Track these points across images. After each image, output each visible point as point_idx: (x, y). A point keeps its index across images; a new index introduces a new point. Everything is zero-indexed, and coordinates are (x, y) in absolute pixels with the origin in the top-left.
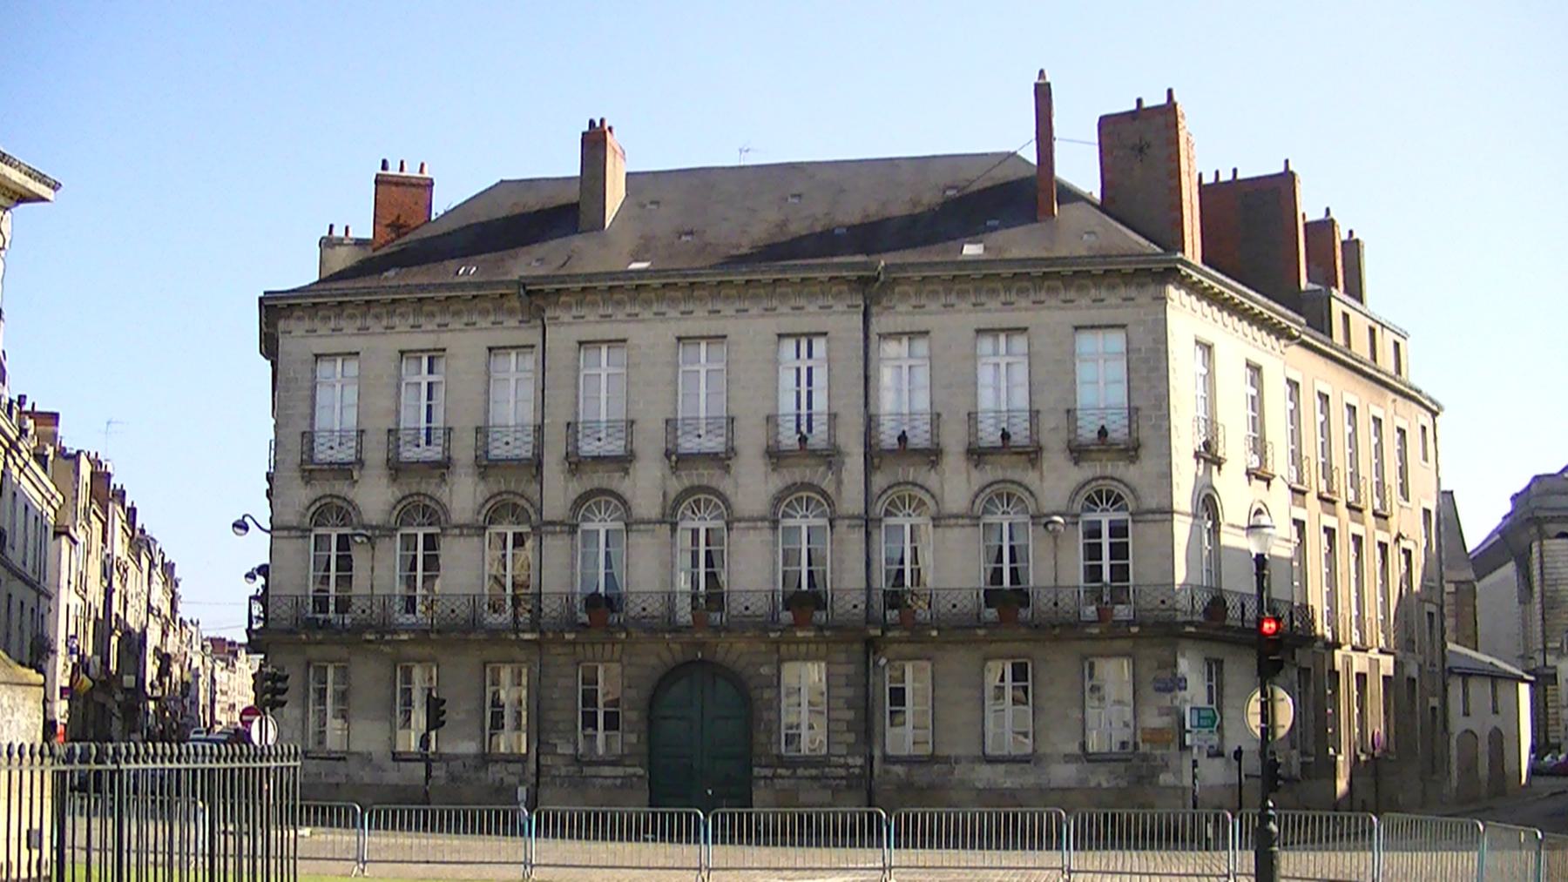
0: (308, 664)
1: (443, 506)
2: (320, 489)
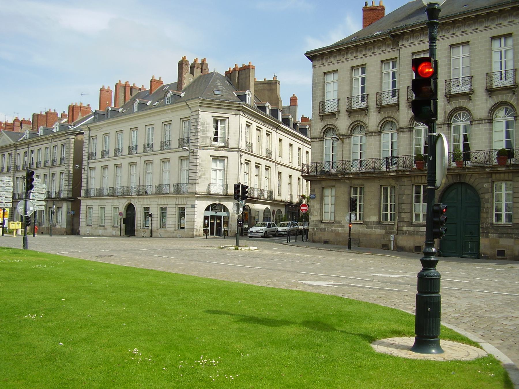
0: (381, 186)
1: (366, 125)
2: (326, 122)
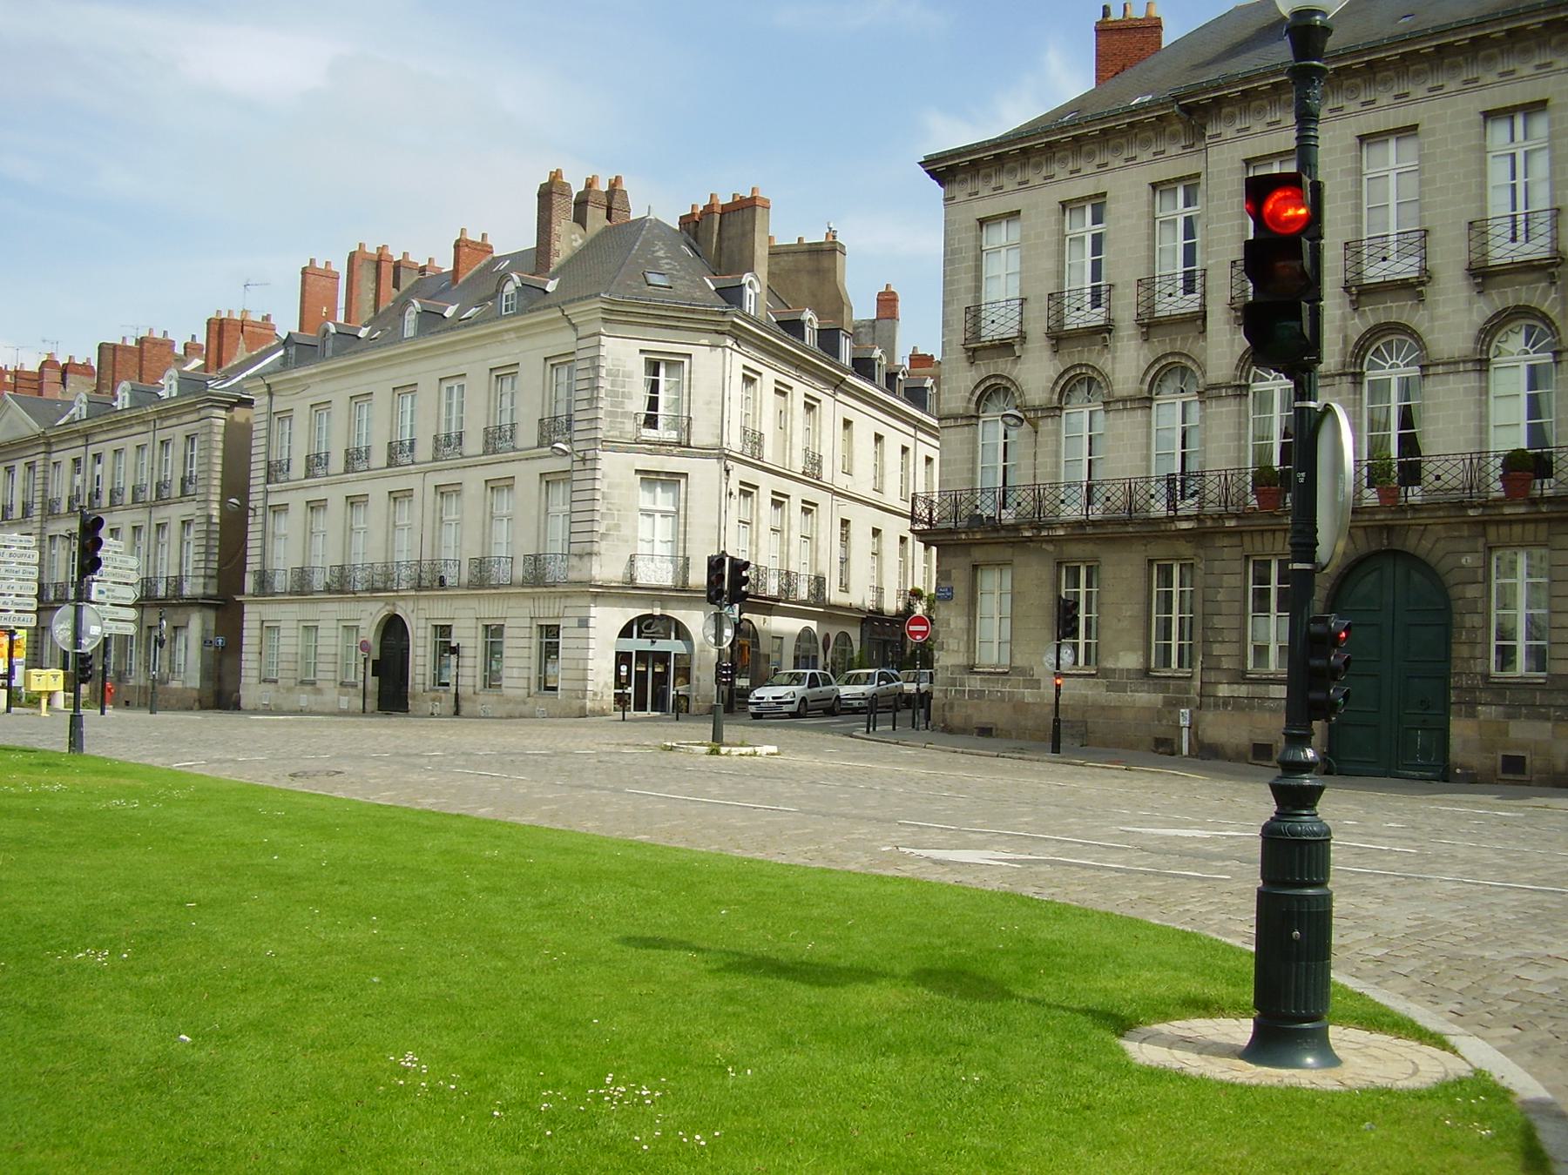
0: (1151, 562)
1: (1106, 377)
2: (985, 368)
